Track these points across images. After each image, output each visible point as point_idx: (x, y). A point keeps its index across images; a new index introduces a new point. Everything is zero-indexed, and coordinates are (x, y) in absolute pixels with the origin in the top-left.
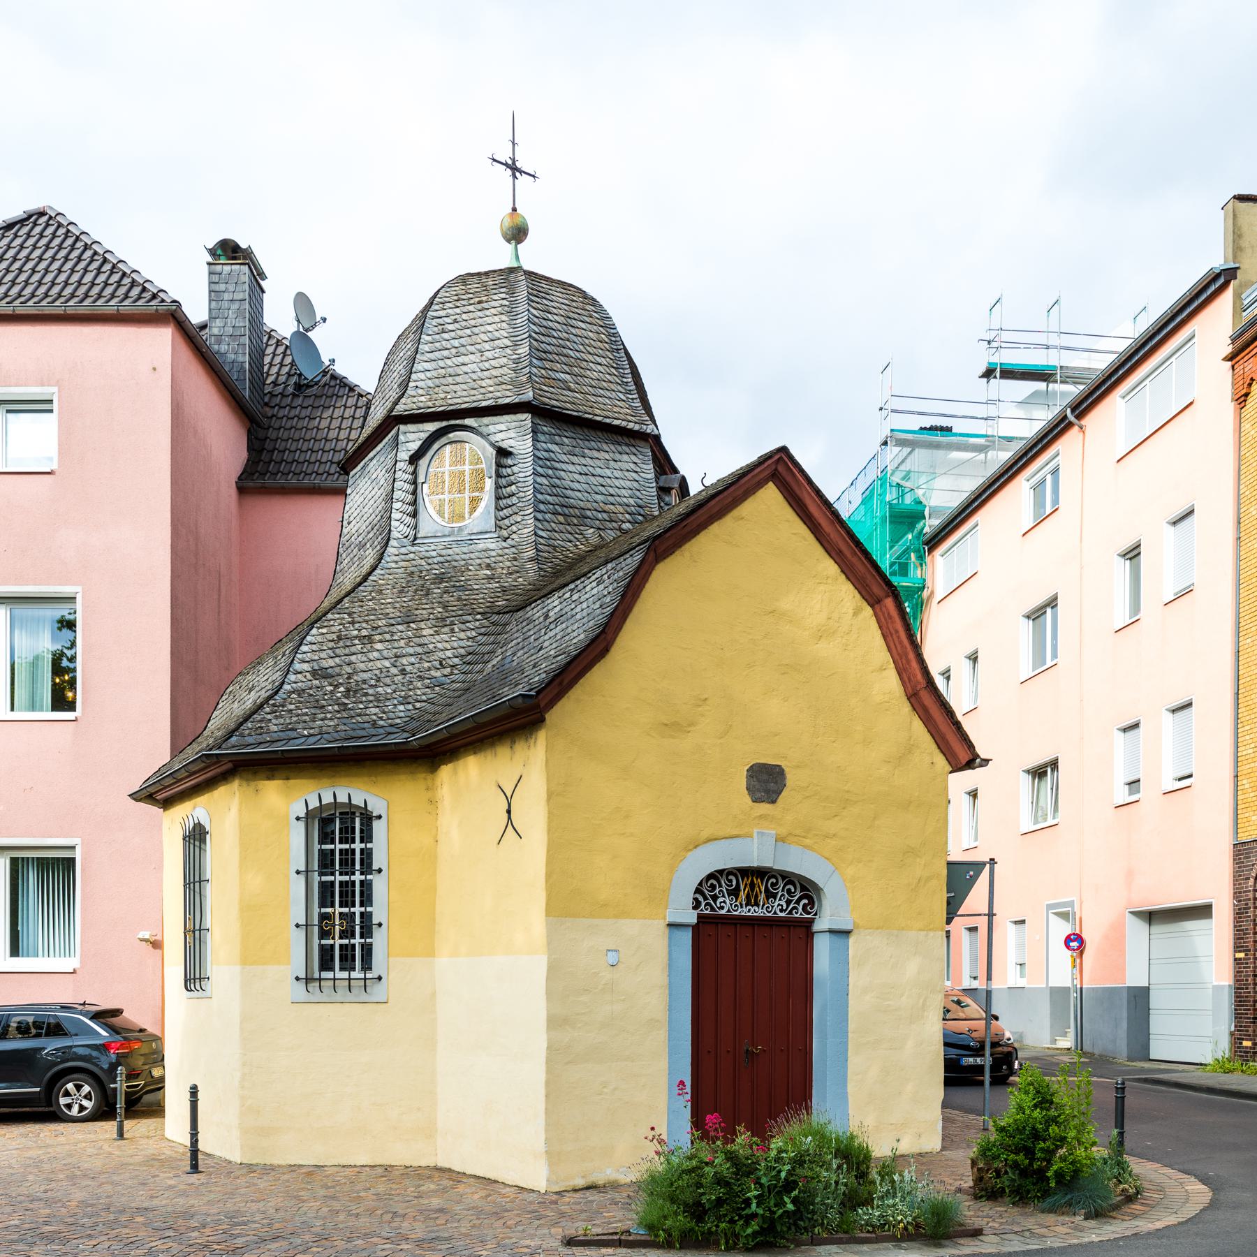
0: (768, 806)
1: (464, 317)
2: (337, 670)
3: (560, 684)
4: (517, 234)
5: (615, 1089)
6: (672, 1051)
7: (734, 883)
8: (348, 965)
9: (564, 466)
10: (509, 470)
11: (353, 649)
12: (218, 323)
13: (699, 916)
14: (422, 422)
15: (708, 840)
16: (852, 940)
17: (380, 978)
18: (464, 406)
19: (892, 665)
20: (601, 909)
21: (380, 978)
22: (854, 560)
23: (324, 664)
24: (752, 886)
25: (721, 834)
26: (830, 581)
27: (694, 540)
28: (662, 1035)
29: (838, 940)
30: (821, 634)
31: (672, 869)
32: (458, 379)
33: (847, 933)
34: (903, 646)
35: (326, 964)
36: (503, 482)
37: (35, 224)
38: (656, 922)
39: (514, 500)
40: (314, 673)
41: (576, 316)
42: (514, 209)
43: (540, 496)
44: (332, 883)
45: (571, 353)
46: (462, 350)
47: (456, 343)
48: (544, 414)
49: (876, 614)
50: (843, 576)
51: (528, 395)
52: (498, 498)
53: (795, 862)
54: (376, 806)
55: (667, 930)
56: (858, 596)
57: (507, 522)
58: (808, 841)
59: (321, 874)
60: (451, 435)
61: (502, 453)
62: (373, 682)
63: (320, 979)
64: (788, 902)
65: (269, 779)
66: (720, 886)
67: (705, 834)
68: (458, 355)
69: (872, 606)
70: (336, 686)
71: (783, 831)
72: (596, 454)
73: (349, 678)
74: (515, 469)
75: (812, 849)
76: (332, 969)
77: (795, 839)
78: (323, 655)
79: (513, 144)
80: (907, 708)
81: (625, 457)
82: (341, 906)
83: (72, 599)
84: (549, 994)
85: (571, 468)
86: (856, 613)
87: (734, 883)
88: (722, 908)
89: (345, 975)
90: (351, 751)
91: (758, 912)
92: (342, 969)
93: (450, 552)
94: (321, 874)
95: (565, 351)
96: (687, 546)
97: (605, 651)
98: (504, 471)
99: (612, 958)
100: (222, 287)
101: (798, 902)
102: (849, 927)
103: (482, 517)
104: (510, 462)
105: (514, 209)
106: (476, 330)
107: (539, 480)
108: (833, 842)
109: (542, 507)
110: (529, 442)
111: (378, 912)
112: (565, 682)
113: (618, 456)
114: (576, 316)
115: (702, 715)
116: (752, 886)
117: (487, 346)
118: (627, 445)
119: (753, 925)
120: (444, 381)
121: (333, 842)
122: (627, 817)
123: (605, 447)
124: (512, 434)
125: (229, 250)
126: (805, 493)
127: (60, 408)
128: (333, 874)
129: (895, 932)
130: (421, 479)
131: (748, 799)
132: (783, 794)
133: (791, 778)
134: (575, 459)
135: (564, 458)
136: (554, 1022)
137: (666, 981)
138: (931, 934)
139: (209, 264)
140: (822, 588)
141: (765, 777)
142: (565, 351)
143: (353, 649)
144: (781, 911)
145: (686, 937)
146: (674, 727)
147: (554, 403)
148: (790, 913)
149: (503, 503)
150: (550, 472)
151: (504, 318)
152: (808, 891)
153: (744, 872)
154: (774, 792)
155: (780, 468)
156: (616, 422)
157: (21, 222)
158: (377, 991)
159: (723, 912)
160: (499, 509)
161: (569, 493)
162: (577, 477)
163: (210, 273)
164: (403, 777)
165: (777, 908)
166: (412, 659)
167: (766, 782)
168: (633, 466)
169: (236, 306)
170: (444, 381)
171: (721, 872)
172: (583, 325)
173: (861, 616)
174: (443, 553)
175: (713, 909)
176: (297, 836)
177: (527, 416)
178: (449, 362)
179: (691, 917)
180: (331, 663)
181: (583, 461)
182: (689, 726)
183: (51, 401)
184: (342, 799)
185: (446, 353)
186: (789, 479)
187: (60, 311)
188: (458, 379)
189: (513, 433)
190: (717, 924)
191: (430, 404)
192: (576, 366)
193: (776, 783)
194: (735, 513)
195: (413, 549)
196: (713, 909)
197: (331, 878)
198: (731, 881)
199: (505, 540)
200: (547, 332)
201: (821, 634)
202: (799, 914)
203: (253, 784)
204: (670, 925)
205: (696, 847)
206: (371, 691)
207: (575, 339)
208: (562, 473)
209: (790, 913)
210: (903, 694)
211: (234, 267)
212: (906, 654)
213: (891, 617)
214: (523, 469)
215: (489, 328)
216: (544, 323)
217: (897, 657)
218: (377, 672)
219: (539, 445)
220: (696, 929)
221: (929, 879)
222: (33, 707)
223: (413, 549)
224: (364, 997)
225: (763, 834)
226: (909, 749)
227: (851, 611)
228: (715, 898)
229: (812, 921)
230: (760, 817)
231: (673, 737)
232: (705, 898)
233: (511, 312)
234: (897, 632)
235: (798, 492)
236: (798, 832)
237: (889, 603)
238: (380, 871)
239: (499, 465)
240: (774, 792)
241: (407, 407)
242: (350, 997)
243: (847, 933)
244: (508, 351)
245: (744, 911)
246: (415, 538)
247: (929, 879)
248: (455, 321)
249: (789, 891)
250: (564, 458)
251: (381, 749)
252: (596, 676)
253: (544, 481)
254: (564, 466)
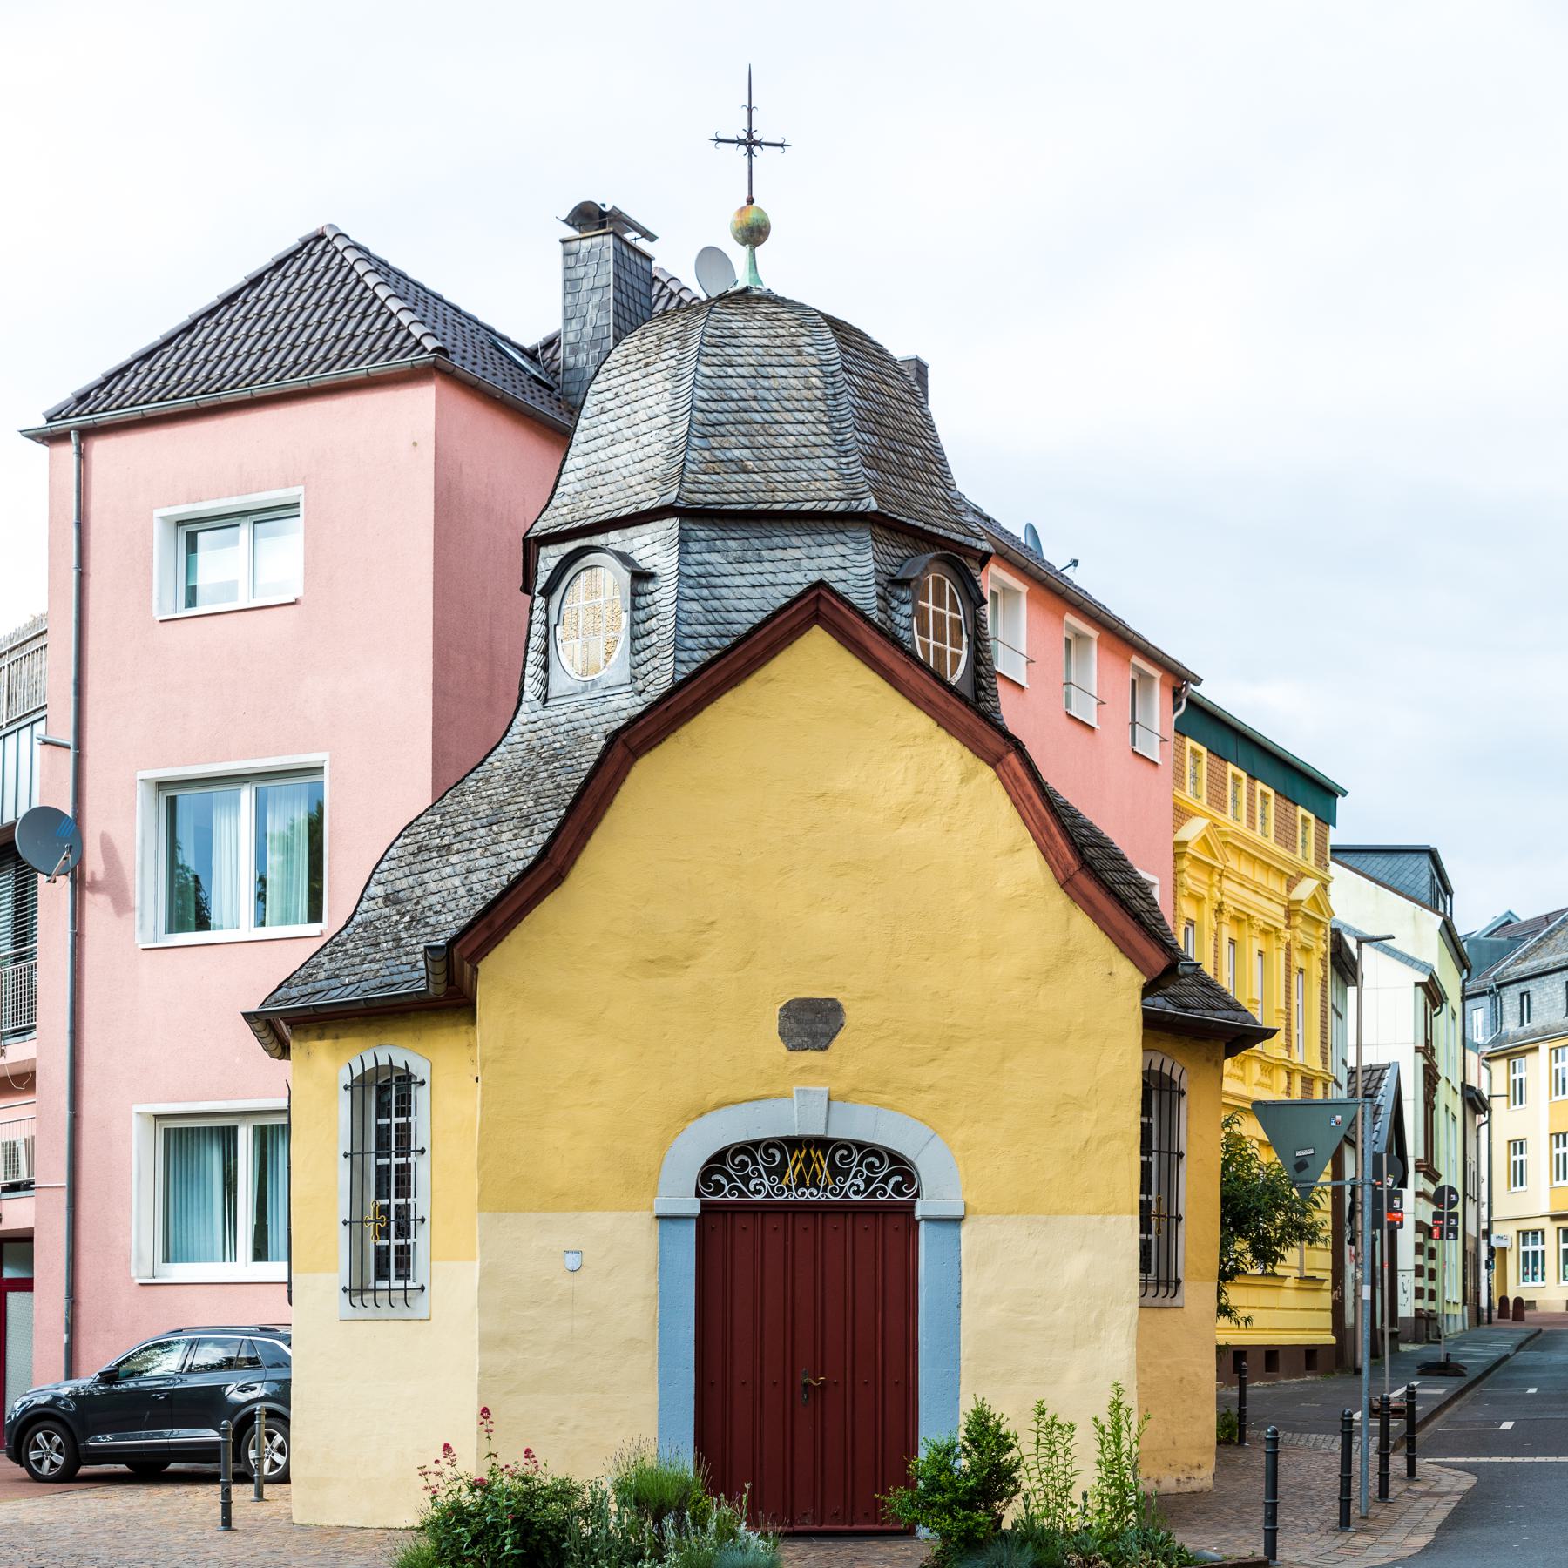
0: (814, 1054)
1: (627, 388)
2: (407, 893)
3: (490, 925)
4: (754, 234)
5: (576, 1427)
6: (664, 1383)
7: (778, 1159)
8: (402, 1272)
9: (726, 581)
10: (649, 599)
11: (428, 865)
12: (575, 325)
13: (704, 1205)
14: (590, 535)
15: (720, 1105)
16: (965, 1230)
17: (423, 1288)
18: (602, 518)
19: (1033, 843)
20: (559, 1200)
21: (423, 1288)
22: (952, 709)
23: (399, 885)
24: (808, 1161)
25: (740, 1095)
26: (919, 741)
27: (694, 720)
28: (645, 1364)
29: (945, 1232)
30: (903, 815)
31: (664, 1145)
32: (608, 478)
33: (958, 1221)
34: (1041, 817)
35: (381, 1274)
36: (641, 615)
37: (310, 254)
38: (637, 1214)
39: (654, 638)
40: (386, 898)
41: (774, 360)
42: (751, 201)
43: (686, 629)
44: (389, 1166)
45: (757, 417)
46: (618, 436)
47: (612, 427)
48: (695, 516)
49: (999, 775)
50: (943, 732)
51: (670, 498)
52: (634, 639)
53: (857, 1124)
54: (419, 1068)
55: (656, 1225)
56: (967, 752)
57: (644, 669)
58: (886, 1098)
59: (378, 1156)
60: (584, 560)
61: (641, 576)
62: (438, 908)
63: (375, 1290)
64: (869, 1182)
65: (320, 1038)
66: (755, 1162)
67: (714, 1097)
68: (613, 443)
69: (993, 766)
70: (403, 915)
71: (840, 1086)
72: (779, 554)
73: (417, 903)
74: (657, 596)
75: (890, 1106)
76: (386, 1277)
77: (864, 1096)
78: (399, 874)
79: (750, 110)
80: (1060, 899)
81: (827, 550)
82: (397, 1197)
83: (319, 770)
84: (483, 1306)
85: (738, 580)
86: (965, 779)
87: (778, 1159)
88: (759, 1192)
89: (400, 1284)
90: (377, 1004)
91: (820, 1196)
92: (398, 1277)
93: (580, 715)
94: (378, 1156)
95: (746, 416)
96: (685, 729)
97: (558, 879)
98: (642, 601)
99: (572, 1261)
100: (580, 272)
101: (885, 1180)
102: (958, 1213)
103: (616, 668)
104: (651, 587)
105: (751, 201)
106: (636, 406)
107: (686, 606)
108: (928, 1097)
109: (689, 643)
110: (675, 557)
111: (420, 1203)
112: (499, 922)
113: (815, 551)
114: (774, 360)
115: (709, 944)
116: (808, 1161)
117: (644, 428)
118: (831, 532)
119: (816, 1213)
120: (593, 482)
121: (389, 1116)
122: (593, 1082)
123: (795, 541)
124: (657, 548)
125: (589, 217)
126: (863, 634)
127: (307, 514)
128: (389, 1156)
129: (1043, 1218)
130: (553, 621)
131: (781, 1048)
132: (838, 1037)
133: (851, 1016)
134: (746, 568)
135: (729, 569)
136: (488, 1342)
137: (653, 1289)
138: (1113, 1219)
139: (564, 242)
140: (906, 752)
141: (810, 1016)
142: (746, 416)
143: (428, 865)
144: (856, 1193)
145: (687, 1235)
146: (661, 963)
147: (712, 498)
148: (873, 1194)
149: (638, 644)
150: (705, 592)
151: (668, 385)
152: (903, 1170)
153: (793, 1143)
154: (823, 1035)
155: (823, 607)
156: (808, 506)
157: (293, 255)
158: (420, 1304)
159: (758, 1197)
160: (635, 653)
161: (734, 616)
162: (746, 591)
163: (566, 255)
164: (445, 1031)
165: (853, 1190)
166: (483, 875)
167: (813, 1023)
168: (838, 561)
169: (595, 298)
170: (593, 482)
171: (756, 1144)
172: (783, 371)
173: (974, 784)
174: (574, 716)
175: (742, 1194)
176: (343, 1106)
177: (675, 521)
178: (602, 455)
179: (693, 1207)
180: (404, 883)
181: (758, 567)
182: (688, 959)
183: (296, 505)
184: (383, 1061)
185: (600, 442)
186: (837, 618)
187: (303, 386)
188: (608, 478)
189: (654, 546)
190: (846, 1213)
191: (569, 518)
192: (758, 434)
193: (827, 1023)
194: (761, 674)
195: (543, 714)
196: (742, 1194)
197: (387, 1161)
198: (773, 1156)
199: (640, 693)
200: (721, 394)
201: (903, 815)
202: (888, 1196)
203: (305, 1045)
204: (661, 1218)
205: (701, 1115)
206: (432, 921)
207: (766, 394)
208: (724, 591)
209: (870, 1195)
210: (1052, 881)
211: (595, 240)
212: (1047, 828)
213: (1018, 779)
214: (664, 594)
215: (650, 402)
216: (719, 383)
217: (1036, 831)
218: (445, 894)
219: (690, 559)
220: (701, 1221)
221: (1103, 1141)
222: (286, 920)
223: (543, 714)
224: (408, 1313)
225: (805, 1092)
226: (1067, 956)
227: (957, 778)
228: (746, 1180)
229: (912, 1206)
230: (803, 1070)
231: (664, 976)
232: (730, 1179)
233: (677, 378)
234: (1030, 798)
235: (854, 634)
236: (867, 1086)
237: (1012, 759)
238: (423, 1151)
239: (635, 594)
240: (823, 1035)
241: (560, 520)
242: (394, 1313)
243: (958, 1221)
244: (665, 432)
245: (793, 1196)
246: (546, 700)
247: (1103, 1141)
248: (617, 395)
249: (870, 1166)
250: (729, 569)
251: (405, 999)
252: (548, 910)
253: (695, 606)
254: (726, 581)
